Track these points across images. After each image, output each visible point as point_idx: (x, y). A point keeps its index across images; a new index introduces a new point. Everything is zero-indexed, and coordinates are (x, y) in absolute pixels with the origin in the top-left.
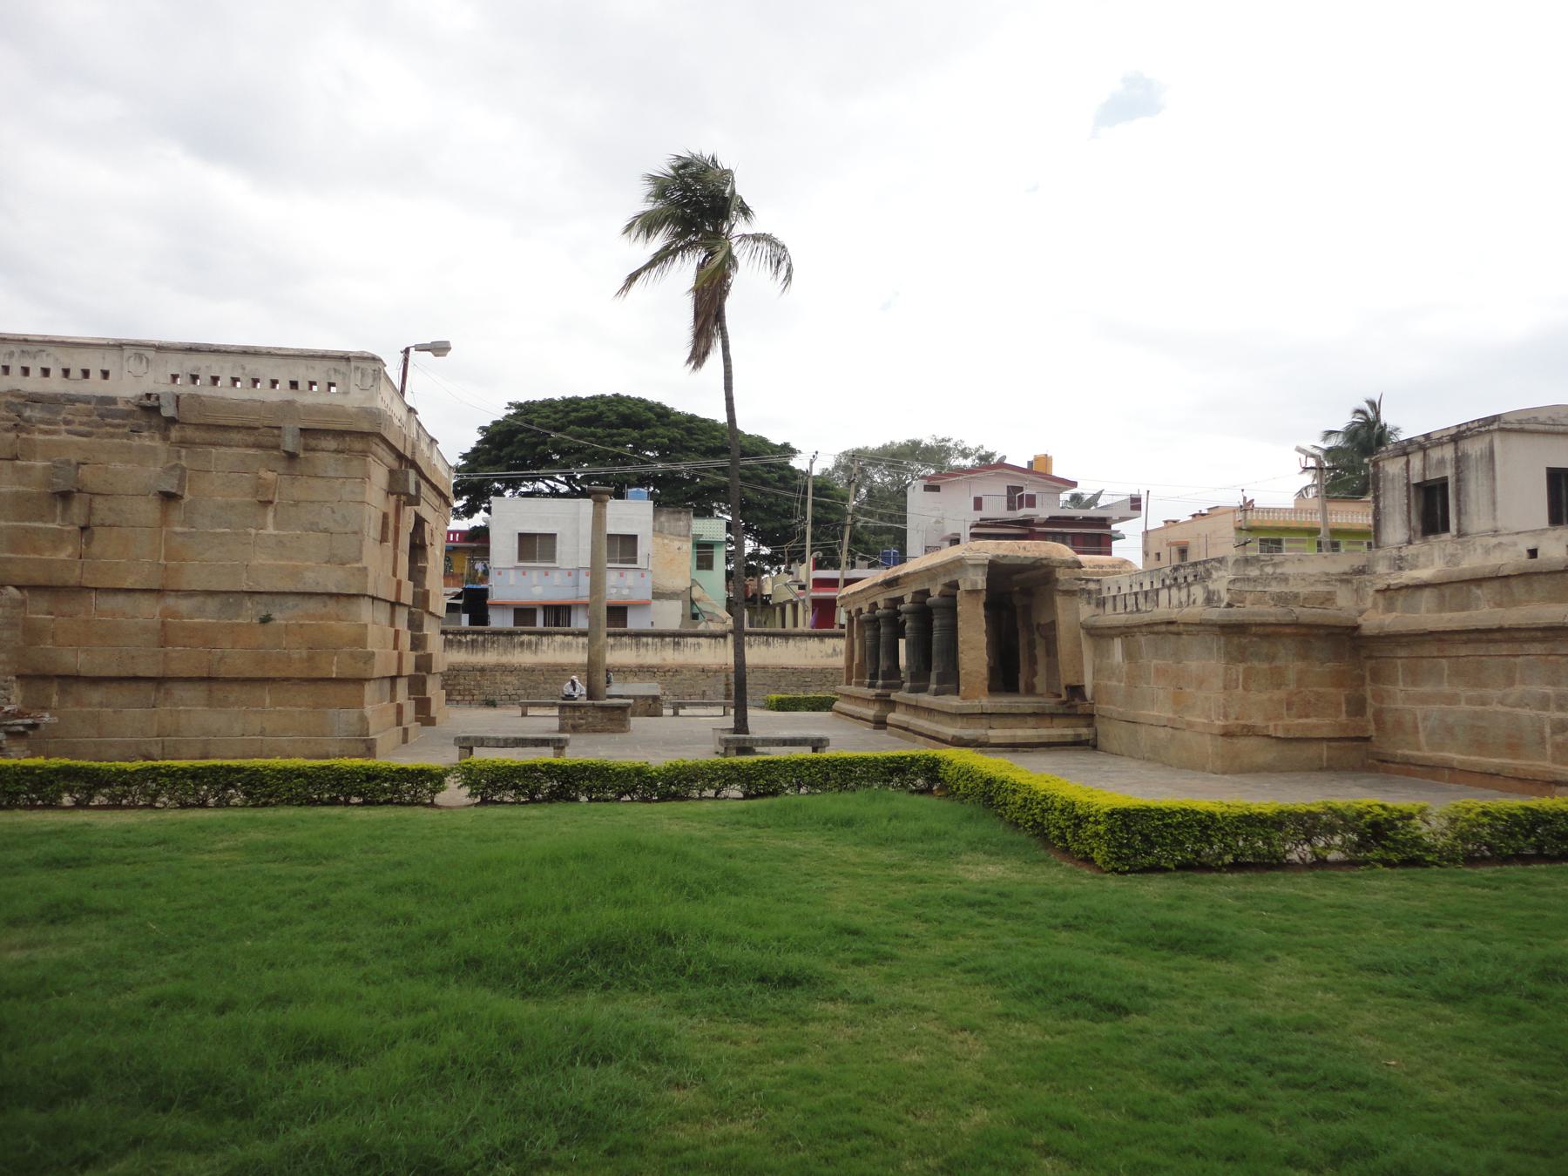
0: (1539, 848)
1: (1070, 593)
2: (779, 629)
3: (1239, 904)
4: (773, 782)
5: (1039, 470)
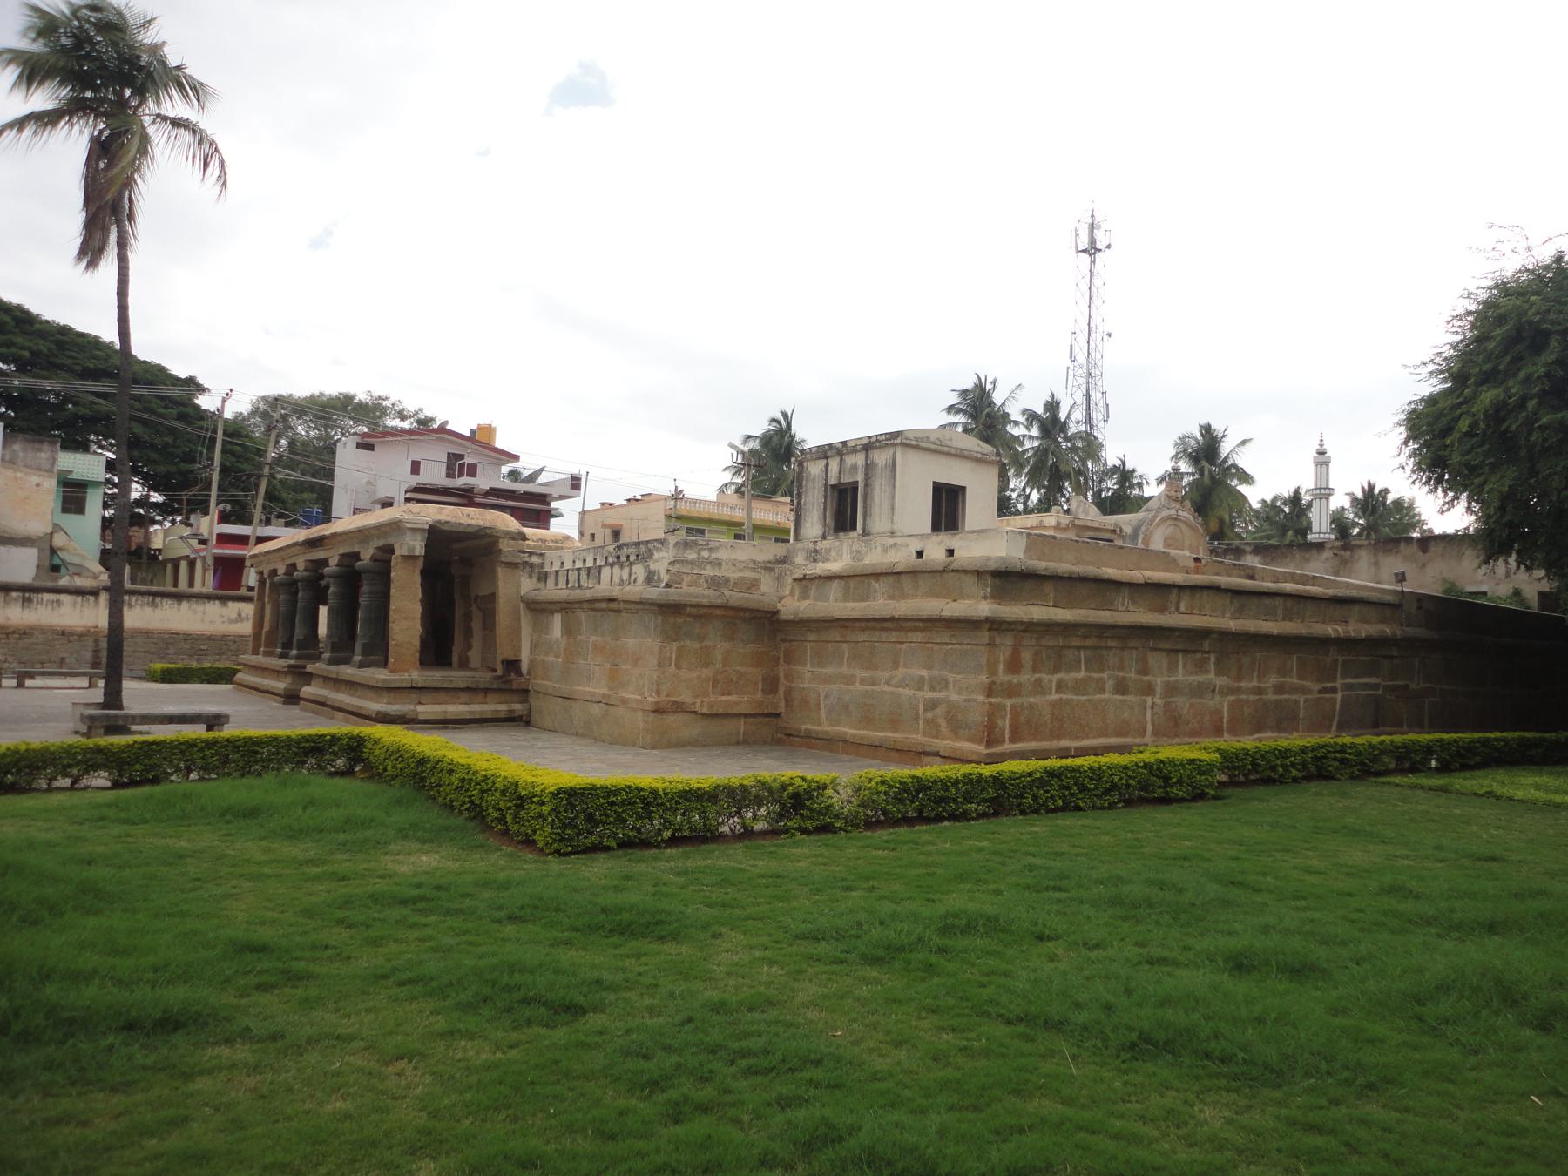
0: (920, 811)
1: (512, 565)
2: (170, 589)
3: (682, 880)
4: (153, 767)
5: (481, 439)
